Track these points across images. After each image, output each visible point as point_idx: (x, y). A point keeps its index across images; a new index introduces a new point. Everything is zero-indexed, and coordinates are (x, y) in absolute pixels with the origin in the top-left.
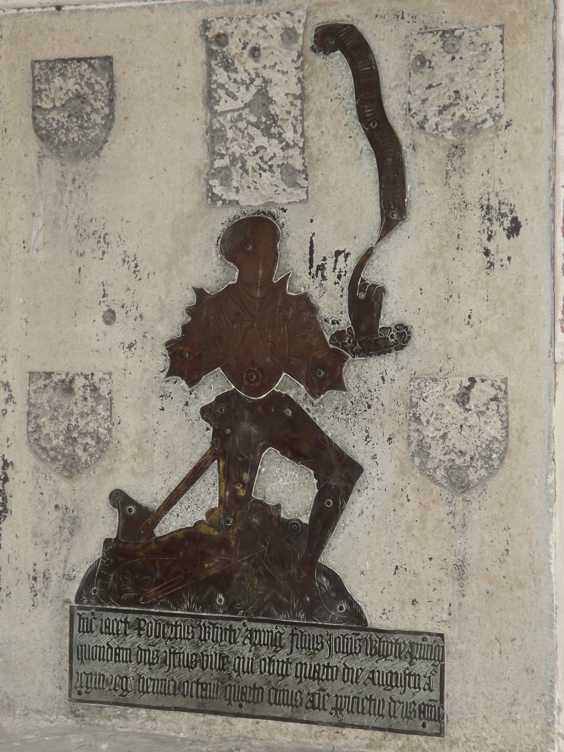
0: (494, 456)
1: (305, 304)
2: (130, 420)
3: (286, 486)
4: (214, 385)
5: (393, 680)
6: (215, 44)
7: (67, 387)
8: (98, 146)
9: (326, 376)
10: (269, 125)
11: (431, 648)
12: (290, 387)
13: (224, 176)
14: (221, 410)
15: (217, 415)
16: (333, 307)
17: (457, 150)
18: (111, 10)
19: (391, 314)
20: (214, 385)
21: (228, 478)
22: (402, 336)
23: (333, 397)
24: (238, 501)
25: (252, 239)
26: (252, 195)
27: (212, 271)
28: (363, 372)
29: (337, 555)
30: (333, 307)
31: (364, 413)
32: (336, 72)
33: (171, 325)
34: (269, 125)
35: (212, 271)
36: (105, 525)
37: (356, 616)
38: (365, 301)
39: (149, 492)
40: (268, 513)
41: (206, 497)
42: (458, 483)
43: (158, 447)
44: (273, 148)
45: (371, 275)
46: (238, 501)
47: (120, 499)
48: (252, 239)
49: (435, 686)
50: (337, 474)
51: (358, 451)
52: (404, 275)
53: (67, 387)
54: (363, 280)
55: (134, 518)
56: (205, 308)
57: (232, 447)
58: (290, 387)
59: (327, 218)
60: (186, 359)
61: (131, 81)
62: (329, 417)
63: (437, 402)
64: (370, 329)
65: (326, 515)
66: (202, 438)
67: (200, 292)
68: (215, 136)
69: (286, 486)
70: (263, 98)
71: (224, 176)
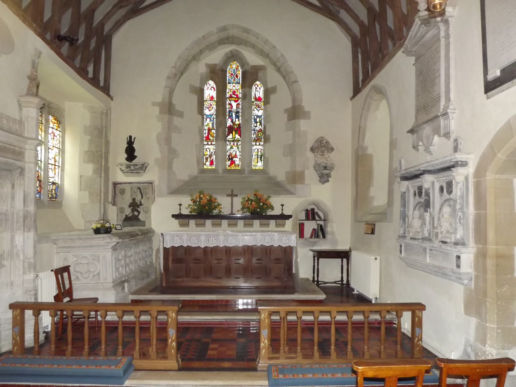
0: (148, 211)
4: (132, 208)
9: (138, 207)
11: (144, 222)
14: (178, 260)
15: (132, 209)
16: (139, 203)
20: (132, 208)
25: (134, 199)
26: (134, 197)
27: (131, 201)
28: (141, 207)
29: (139, 217)
30: (139, 203)
31: (140, 209)
33: (129, 204)
35: (131, 201)
36: (124, 216)
38: (141, 203)
39: (127, 214)
41: (131, 214)
42: (146, 212)
43: (128, 212)
48: (134, 199)
49: (117, 192)
50: (139, 212)
52: (143, 201)
54: (199, 174)
56: (131, 203)
57: (133, 211)
59: (138, 198)
60: (130, 206)
61: (126, 190)
62: (139, 209)
63: (145, 209)
64: (141, 204)
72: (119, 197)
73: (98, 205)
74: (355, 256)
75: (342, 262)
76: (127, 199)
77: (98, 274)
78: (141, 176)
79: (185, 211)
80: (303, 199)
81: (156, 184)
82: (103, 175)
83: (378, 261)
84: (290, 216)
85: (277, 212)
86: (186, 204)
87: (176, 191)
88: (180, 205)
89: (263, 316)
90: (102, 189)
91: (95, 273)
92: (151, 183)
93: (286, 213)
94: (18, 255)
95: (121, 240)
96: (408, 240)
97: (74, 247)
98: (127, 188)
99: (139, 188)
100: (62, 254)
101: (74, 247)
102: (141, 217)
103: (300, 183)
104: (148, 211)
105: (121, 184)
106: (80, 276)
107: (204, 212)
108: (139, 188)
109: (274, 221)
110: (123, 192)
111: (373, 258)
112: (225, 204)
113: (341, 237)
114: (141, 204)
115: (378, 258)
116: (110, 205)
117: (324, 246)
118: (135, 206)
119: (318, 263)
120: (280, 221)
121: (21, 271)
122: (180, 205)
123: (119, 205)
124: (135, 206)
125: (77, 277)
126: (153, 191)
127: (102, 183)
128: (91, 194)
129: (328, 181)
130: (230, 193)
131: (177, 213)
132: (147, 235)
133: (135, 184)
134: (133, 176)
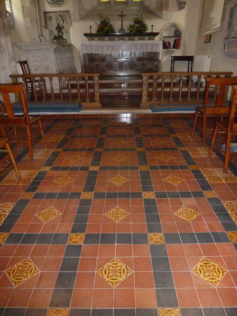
25: (58, 24)
26: (58, 22)
31: (63, 31)
38: (63, 26)
43: (56, 33)
48: (58, 24)
52: (64, 25)
57: (59, 32)
59: (61, 23)
64: (63, 28)
72: (49, 23)
73: (37, 28)
74: (195, 59)
75: (189, 63)
76: (53, 24)
77: (48, 67)
78: (61, 6)
79: (94, 31)
80: (166, 22)
81: (72, 12)
82: (37, 6)
83: (210, 58)
84: (158, 34)
85: (149, 31)
86: (93, 26)
87: (85, 17)
88: (91, 27)
89: (144, 79)
90: (38, 18)
91: (46, 66)
92: (69, 12)
93: (154, 31)
94: (5, 51)
95: (58, 46)
96: (230, 39)
97: (32, 50)
98: (53, 15)
99: (61, 16)
100: (25, 55)
101: (32, 50)
102: (64, 36)
103: (166, 10)
104: (68, 32)
105: (48, 13)
106: (38, 69)
107: (105, 31)
108: (61, 16)
109: (147, 37)
110: (51, 19)
111: (208, 56)
112: (116, 25)
113: (189, 47)
114: (63, 28)
115: (211, 57)
116: (44, 28)
117: (178, 53)
118: (59, 28)
119: (174, 63)
120: (151, 37)
121: (8, 62)
122: (91, 27)
123: (50, 29)
124: (59, 28)
125: (36, 69)
126: (70, 17)
127: (37, 12)
128: (31, 20)
129: (184, 8)
130: (121, 14)
131: (89, 32)
132: (71, 47)
133: (58, 13)
134: (56, 7)
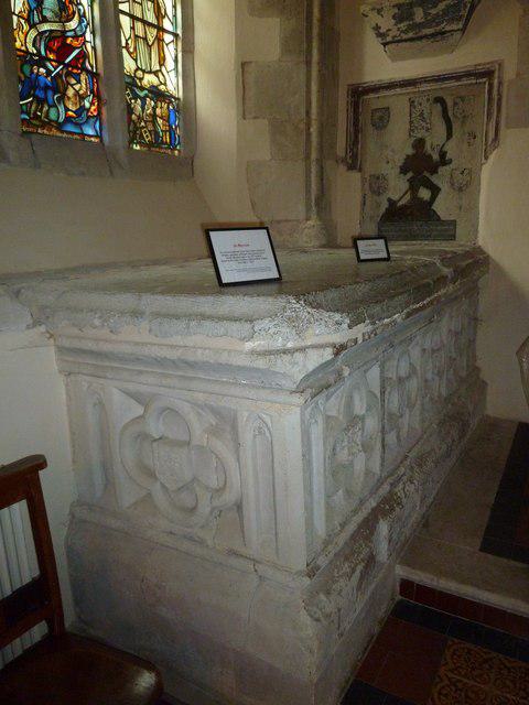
0: (468, 184)
1: (430, 156)
2: (392, 183)
3: (425, 194)
4: (410, 175)
5: (446, 230)
6: (412, 103)
7: (378, 178)
8: (385, 127)
9: (434, 171)
10: (423, 119)
12: (428, 175)
13: (413, 131)
15: (411, 181)
16: (436, 157)
17: (463, 122)
18: (309, 134)
19: (448, 157)
20: (410, 175)
21: (412, 194)
22: (450, 161)
23: (435, 175)
24: (415, 197)
25: (419, 144)
27: (410, 151)
28: (443, 170)
29: (435, 207)
30: (436, 157)
31: (441, 179)
32: (439, 107)
34: (423, 119)
36: (385, 205)
37: (439, 219)
38: (443, 155)
40: (421, 200)
41: (408, 197)
42: (460, 189)
44: (424, 124)
45: (445, 149)
46: (415, 197)
47: (389, 200)
48: (419, 144)
50: (435, 190)
51: (440, 186)
53: (378, 178)
55: (392, 203)
57: (413, 188)
58: (428, 175)
59: (435, 138)
60: (404, 170)
62: (434, 179)
64: (444, 160)
65: (433, 198)
66: (407, 185)
67: (408, 156)
68: (411, 122)
69: (425, 194)
70: (422, 114)
71: (413, 131)
